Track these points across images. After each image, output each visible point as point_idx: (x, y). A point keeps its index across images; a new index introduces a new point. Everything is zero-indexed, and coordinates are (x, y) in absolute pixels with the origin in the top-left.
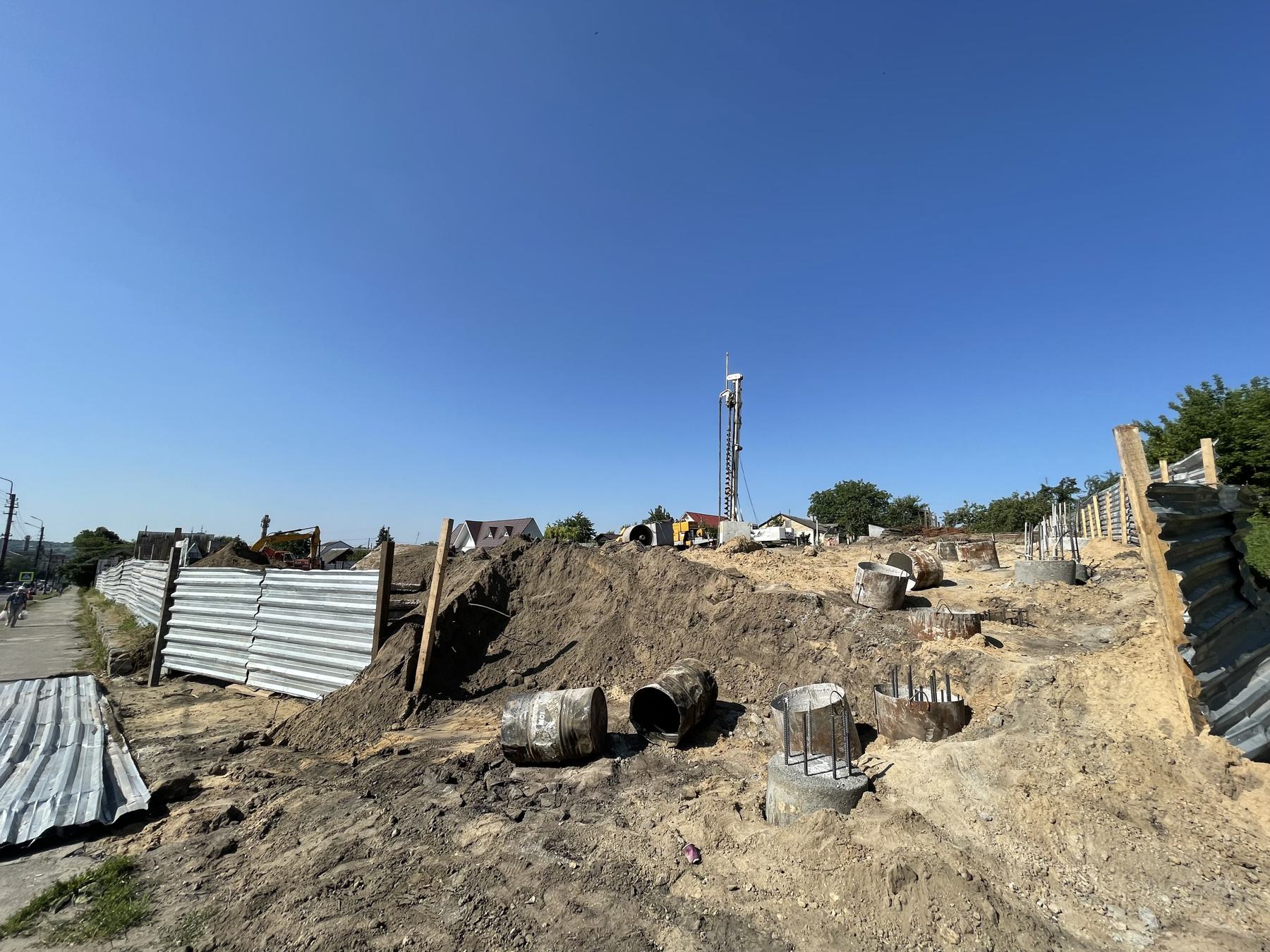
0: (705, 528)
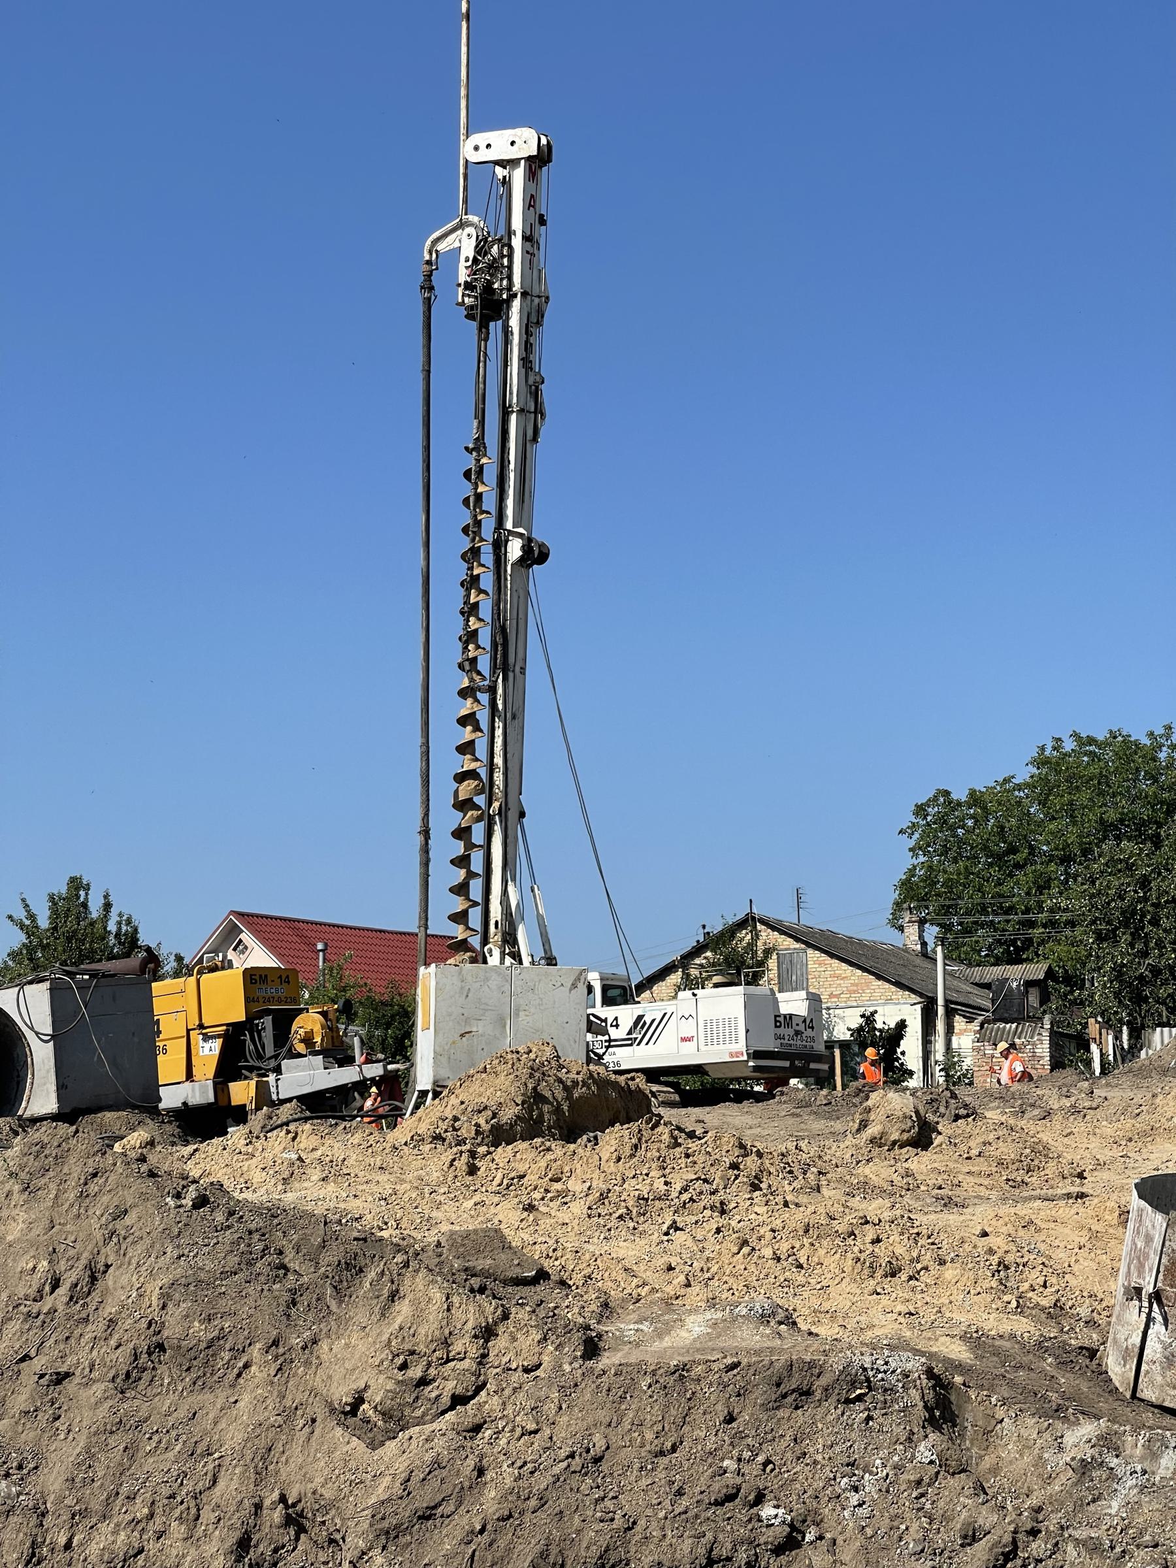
0: (335, 1011)
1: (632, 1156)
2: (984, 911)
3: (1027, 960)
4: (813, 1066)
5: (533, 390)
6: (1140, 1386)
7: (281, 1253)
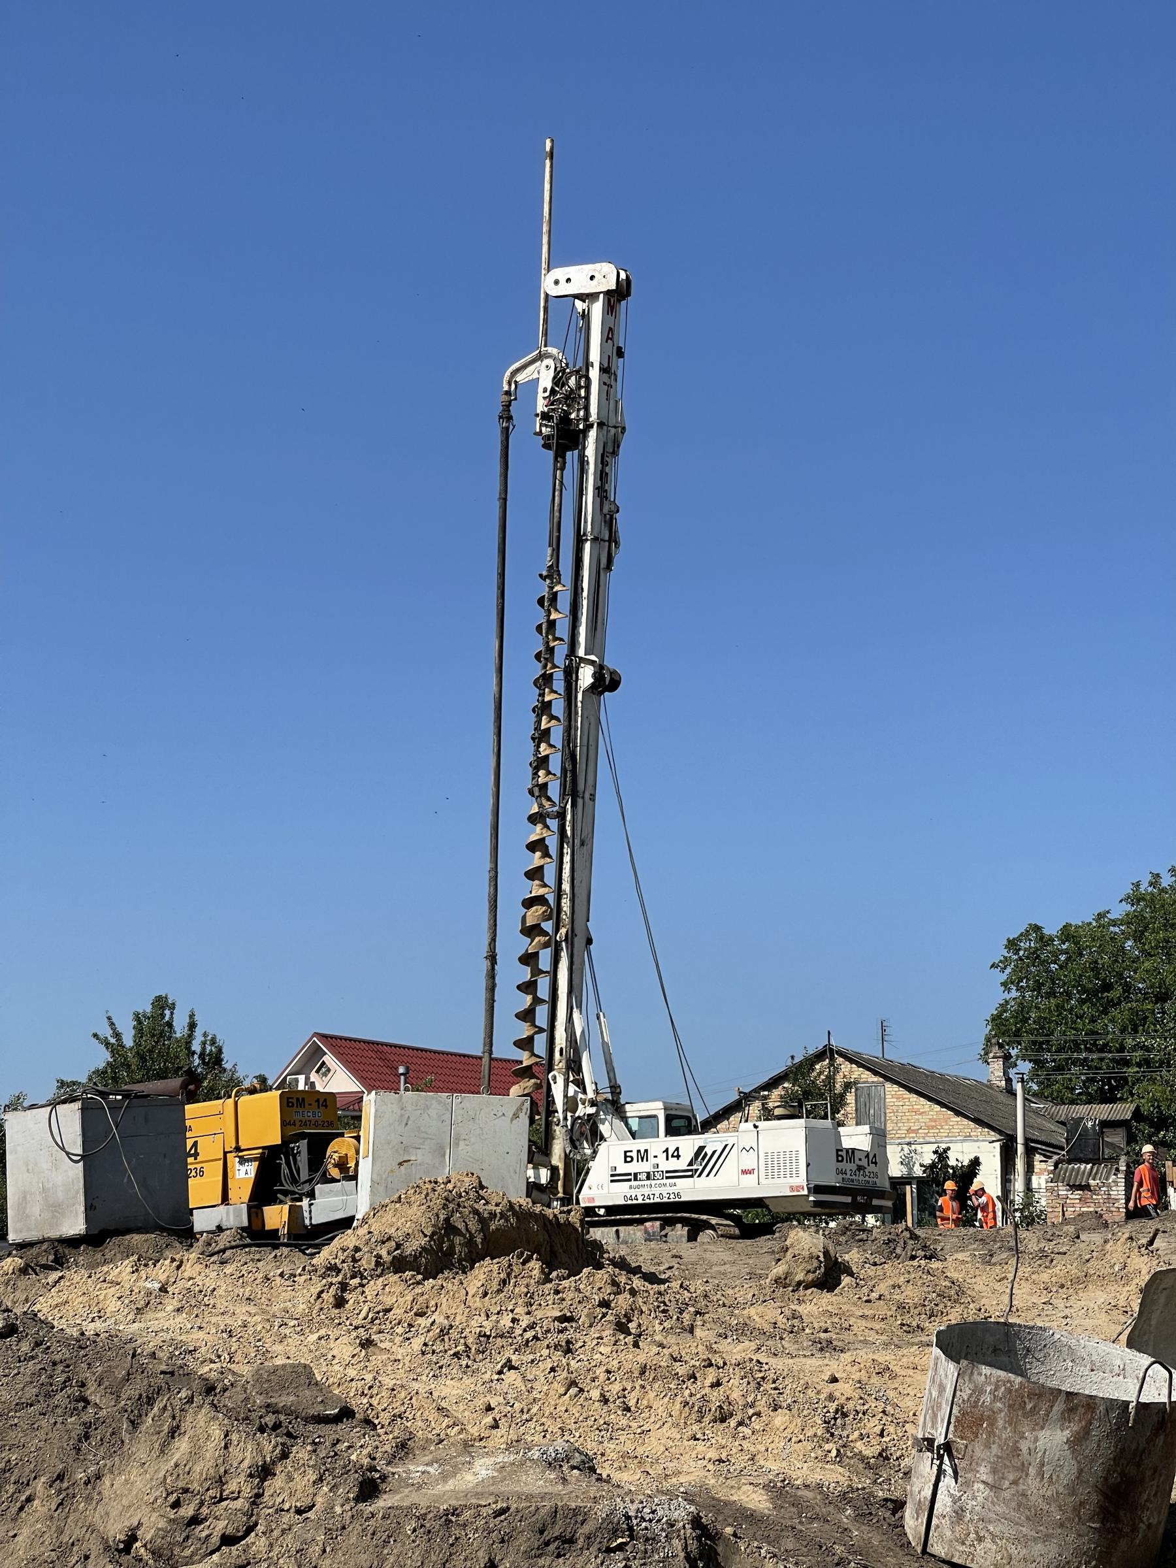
1: (499, 1291)
2: (1076, 1046)
3: (1121, 1099)
4: (875, 1202)
5: (608, 519)
6: (931, 1541)
7: (83, 1385)
